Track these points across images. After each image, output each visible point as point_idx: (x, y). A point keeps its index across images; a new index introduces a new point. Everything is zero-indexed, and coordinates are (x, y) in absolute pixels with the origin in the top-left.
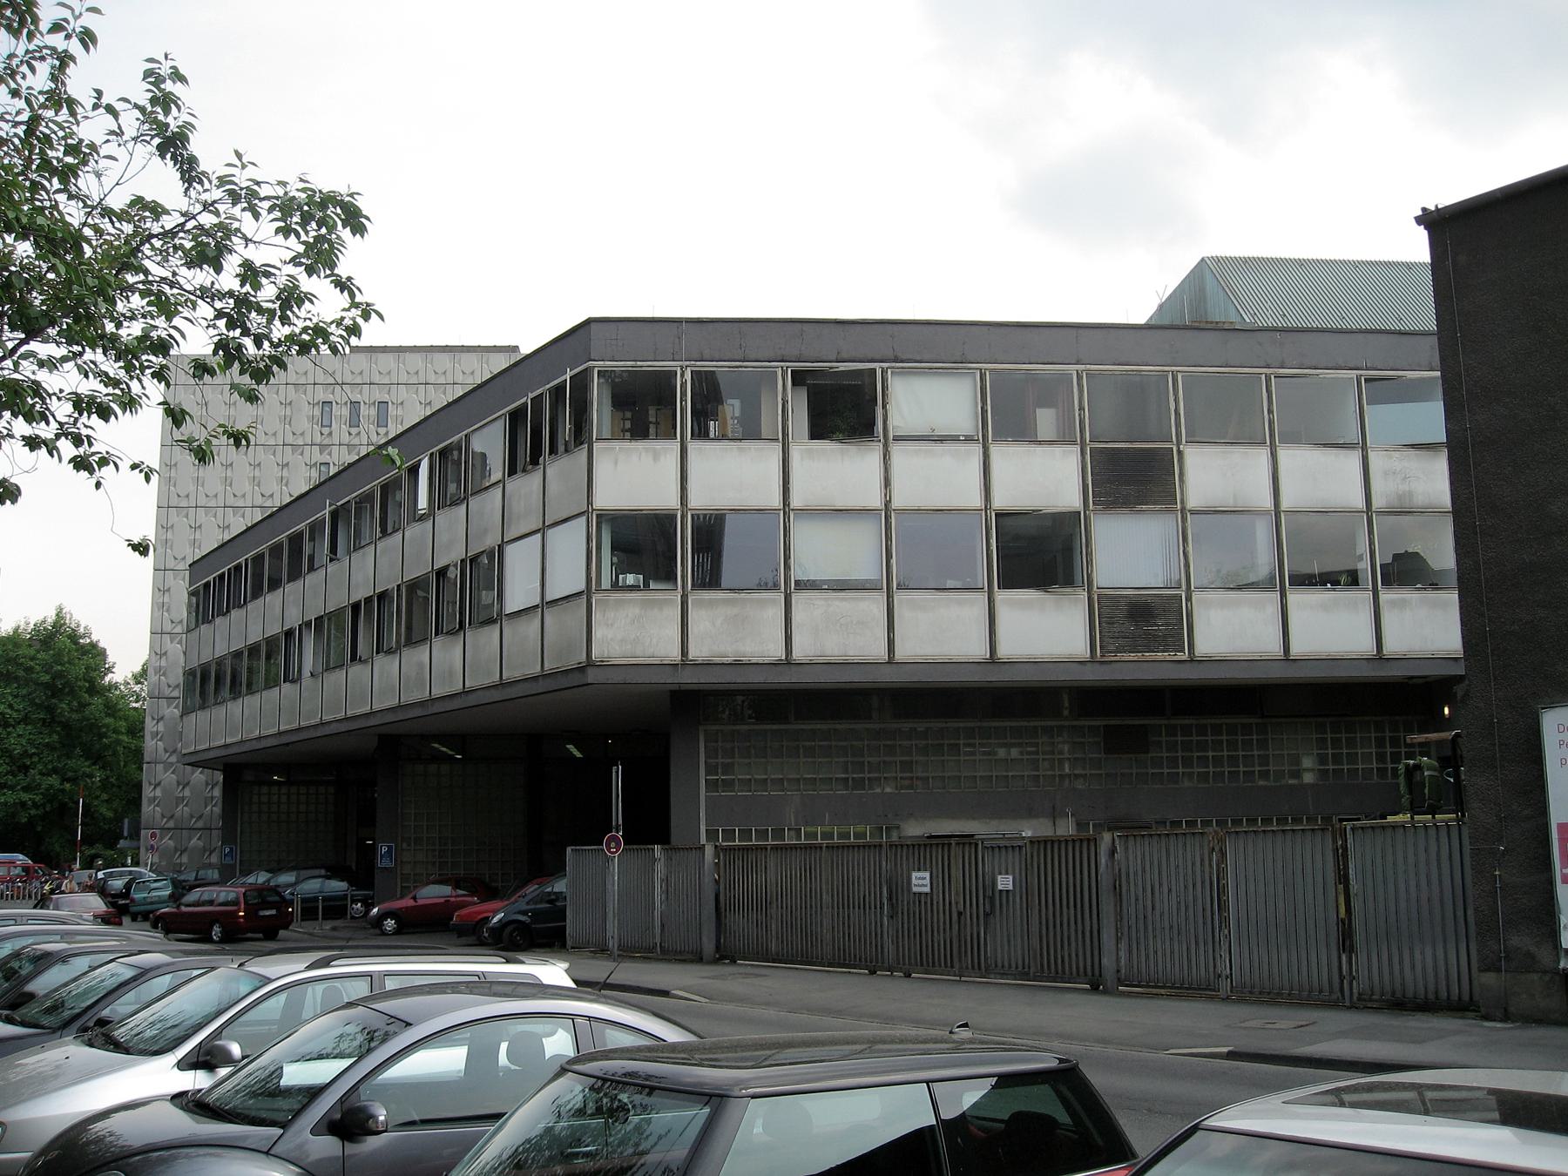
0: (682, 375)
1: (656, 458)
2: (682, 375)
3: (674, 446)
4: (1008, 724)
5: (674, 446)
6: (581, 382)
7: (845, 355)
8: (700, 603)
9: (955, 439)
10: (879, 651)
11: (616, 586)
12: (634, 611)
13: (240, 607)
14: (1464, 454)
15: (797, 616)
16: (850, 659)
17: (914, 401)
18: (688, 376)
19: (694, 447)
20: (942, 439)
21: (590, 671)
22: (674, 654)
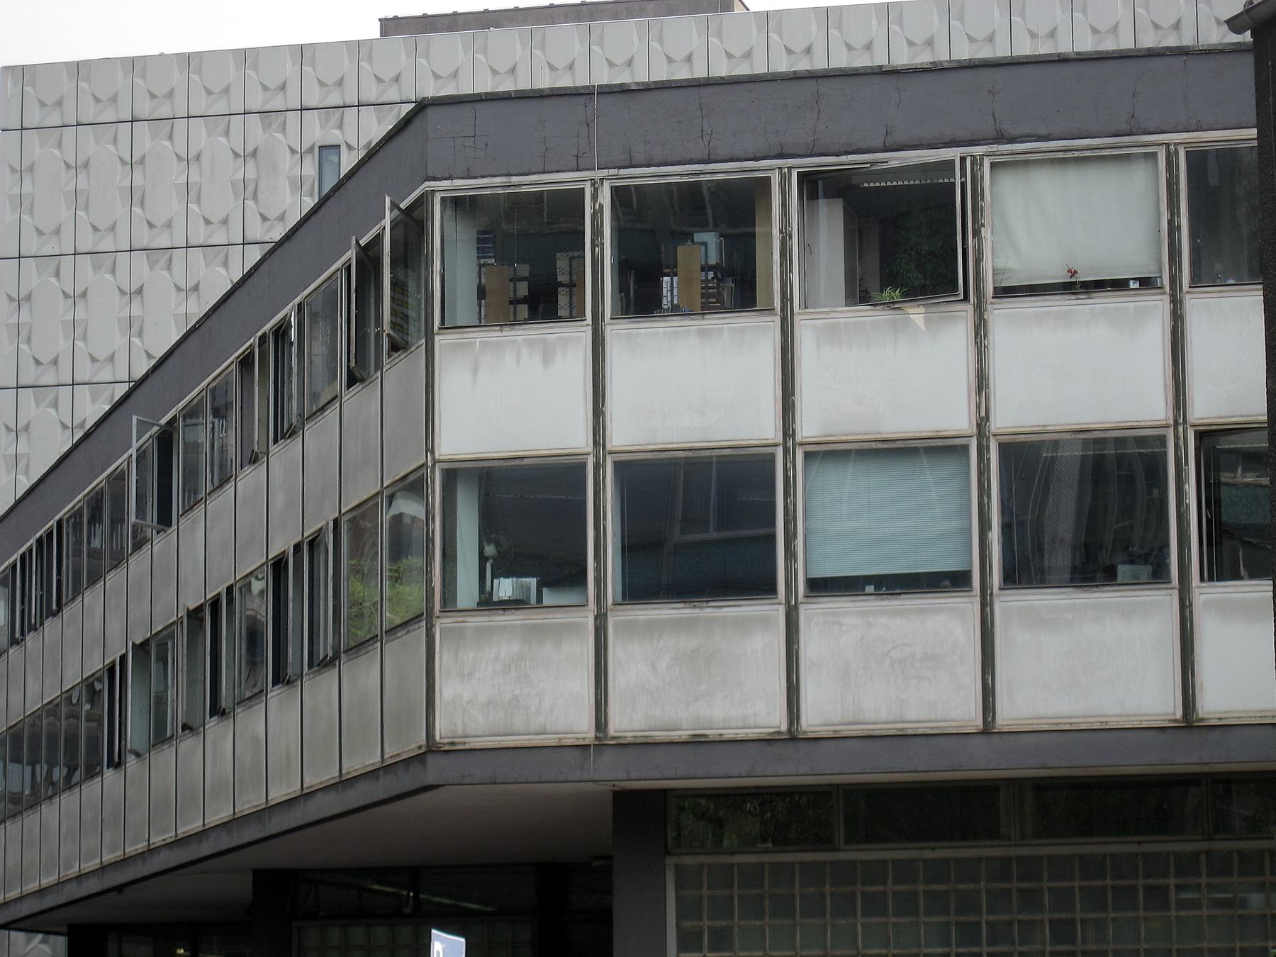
0: (595, 197)
1: (547, 358)
2: (595, 197)
3: (581, 334)
4: (889, 855)
5: (581, 334)
6: (412, 224)
7: (900, 137)
8: (630, 629)
9: (1119, 285)
10: (962, 709)
11: (487, 603)
12: (508, 648)
13: (54, 615)
14: (507, 577)
15: (618, 679)
16: (910, 728)
17: (1031, 216)
18: (605, 198)
19: (620, 334)
20: (1074, 287)
21: (432, 761)
22: (581, 726)
